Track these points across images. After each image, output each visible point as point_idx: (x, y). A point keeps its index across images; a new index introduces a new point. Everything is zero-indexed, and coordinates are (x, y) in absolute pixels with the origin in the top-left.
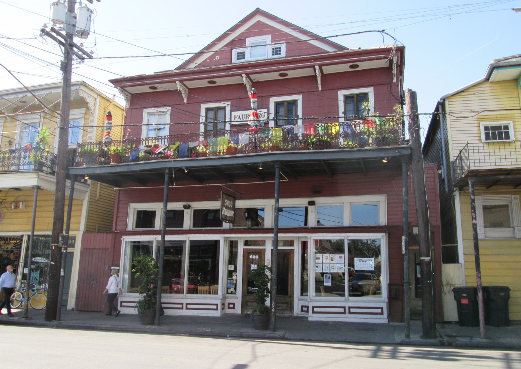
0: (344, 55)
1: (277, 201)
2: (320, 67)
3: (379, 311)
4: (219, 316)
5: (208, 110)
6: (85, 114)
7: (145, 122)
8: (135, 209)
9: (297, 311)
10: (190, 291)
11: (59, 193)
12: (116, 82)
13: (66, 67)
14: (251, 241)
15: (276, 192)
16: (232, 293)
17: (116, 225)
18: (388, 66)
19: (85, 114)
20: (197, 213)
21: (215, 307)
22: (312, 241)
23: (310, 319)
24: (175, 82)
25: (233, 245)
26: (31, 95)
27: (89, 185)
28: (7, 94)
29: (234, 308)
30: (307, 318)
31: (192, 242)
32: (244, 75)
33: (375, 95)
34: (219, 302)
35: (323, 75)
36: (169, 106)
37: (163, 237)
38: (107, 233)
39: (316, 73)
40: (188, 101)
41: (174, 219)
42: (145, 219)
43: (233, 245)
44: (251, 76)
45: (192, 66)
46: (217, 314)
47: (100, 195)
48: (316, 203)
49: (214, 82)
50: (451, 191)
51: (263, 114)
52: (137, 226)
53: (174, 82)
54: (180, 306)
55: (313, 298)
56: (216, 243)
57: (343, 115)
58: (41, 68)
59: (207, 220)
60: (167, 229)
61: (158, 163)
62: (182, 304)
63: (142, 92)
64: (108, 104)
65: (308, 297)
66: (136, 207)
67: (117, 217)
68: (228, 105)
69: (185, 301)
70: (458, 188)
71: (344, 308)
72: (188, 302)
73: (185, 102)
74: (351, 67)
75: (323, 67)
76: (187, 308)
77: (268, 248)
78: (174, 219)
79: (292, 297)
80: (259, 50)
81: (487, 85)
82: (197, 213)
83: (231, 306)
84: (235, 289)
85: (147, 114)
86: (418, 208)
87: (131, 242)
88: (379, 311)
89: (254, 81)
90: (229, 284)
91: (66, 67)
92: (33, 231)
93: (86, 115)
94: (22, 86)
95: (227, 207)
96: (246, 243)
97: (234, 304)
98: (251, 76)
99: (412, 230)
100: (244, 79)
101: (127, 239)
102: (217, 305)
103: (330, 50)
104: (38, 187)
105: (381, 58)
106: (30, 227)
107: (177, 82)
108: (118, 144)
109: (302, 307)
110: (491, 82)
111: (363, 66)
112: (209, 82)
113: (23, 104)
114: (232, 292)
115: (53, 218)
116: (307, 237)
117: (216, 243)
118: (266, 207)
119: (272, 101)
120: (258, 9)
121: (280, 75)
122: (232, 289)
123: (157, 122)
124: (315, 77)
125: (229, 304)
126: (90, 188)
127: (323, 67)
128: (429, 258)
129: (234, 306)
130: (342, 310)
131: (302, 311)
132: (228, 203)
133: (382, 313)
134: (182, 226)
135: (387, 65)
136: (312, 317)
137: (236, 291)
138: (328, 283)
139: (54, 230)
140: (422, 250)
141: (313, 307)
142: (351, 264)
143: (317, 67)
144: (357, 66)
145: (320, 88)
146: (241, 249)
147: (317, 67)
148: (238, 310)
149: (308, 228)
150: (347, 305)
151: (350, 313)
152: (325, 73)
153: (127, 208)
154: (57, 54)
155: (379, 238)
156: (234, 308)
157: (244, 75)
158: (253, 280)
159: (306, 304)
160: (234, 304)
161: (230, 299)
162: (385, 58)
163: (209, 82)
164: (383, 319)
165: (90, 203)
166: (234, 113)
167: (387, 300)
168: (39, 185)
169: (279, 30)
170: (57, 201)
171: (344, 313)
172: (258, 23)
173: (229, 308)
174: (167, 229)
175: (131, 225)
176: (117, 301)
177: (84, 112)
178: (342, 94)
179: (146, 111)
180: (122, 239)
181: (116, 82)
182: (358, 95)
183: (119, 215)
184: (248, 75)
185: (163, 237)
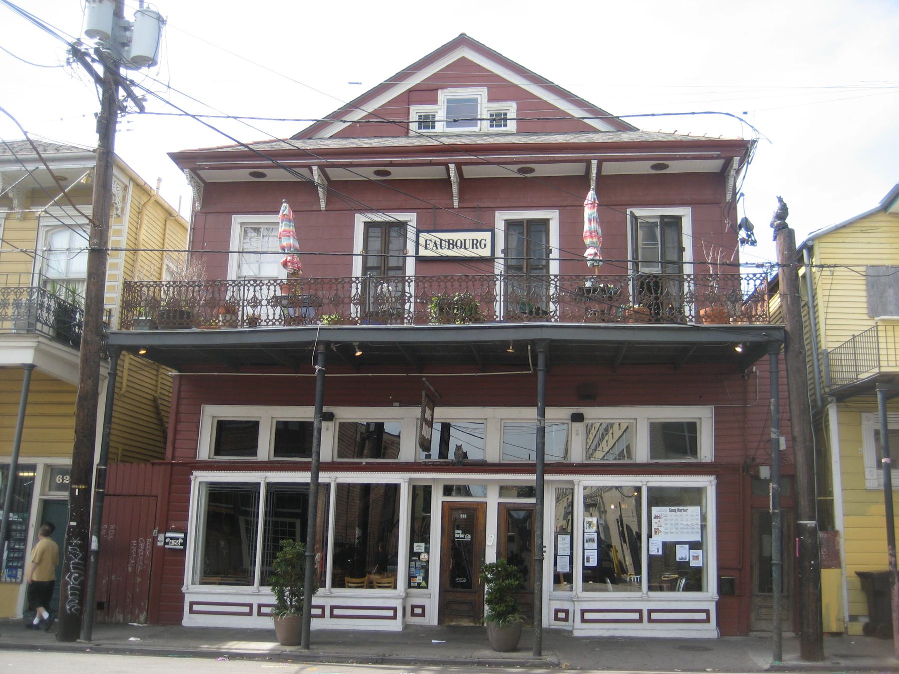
1: (542, 414)
2: (459, 166)
5: (368, 226)
6: (6, 219)
7: (234, 245)
8: (213, 417)
9: (547, 620)
11: (90, 382)
12: (183, 159)
16: (419, 586)
17: (174, 449)
18: (582, 173)
19: (6, 219)
20: (346, 431)
23: (577, 634)
25: (422, 495)
26: (45, 167)
29: (566, 619)
30: (571, 632)
31: (269, 485)
33: (694, 221)
34: (398, 604)
35: (464, 182)
37: (315, 477)
38: (153, 464)
39: (450, 177)
42: (236, 440)
43: (422, 495)
44: (328, 170)
46: (396, 626)
49: (263, 175)
50: (825, 403)
51: (483, 242)
52: (277, 452)
54: (247, 609)
55: (585, 597)
56: (395, 488)
57: (502, 256)
58: (64, 115)
59: (373, 444)
61: (578, 330)
63: (232, 181)
64: (145, 199)
65: (574, 592)
66: (213, 413)
67: (176, 432)
68: (410, 218)
70: (834, 399)
71: (640, 612)
72: (261, 602)
73: (456, 205)
74: (654, 167)
75: (464, 168)
77: (493, 503)
78: (295, 441)
80: (488, 121)
81: (882, 217)
82: (346, 431)
83: (418, 611)
84: (426, 578)
85: (239, 226)
86: (796, 434)
87: (207, 483)
88: (703, 616)
89: (333, 179)
90: (413, 570)
93: (7, 221)
94: (234, 143)
96: (448, 490)
97: (423, 608)
98: (328, 170)
99: (758, 472)
101: (200, 478)
102: (707, 612)
104: (31, 367)
105: (712, 158)
109: (557, 611)
110: (890, 213)
111: (676, 167)
112: (252, 174)
113: (41, 184)
114: (419, 584)
115: (73, 431)
116: (572, 482)
117: (395, 488)
118: (400, 421)
119: (501, 218)
120: (462, 34)
122: (419, 579)
123: (262, 255)
124: (448, 182)
127: (464, 168)
128: (814, 522)
130: (636, 616)
131: (556, 618)
133: (707, 620)
134: (255, 454)
135: (582, 173)
136: (582, 630)
137: (427, 583)
139: (76, 456)
141: (583, 612)
142: (7, 517)
143: (594, 163)
144: (666, 167)
146: (438, 500)
147: (594, 163)
148: (432, 618)
149: (571, 465)
150: (645, 607)
151: (650, 620)
152: (466, 176)
153: (198, 414)
156: (423, 615)
157: (315, 168)
158: (461, 561)
159: (566, 605)
161: (418, 598)
162: (718, 157)
163: (252, 174)
164: (710, 630)
166: (423, 236)
167: (716, 597)
168: (35, 364)
169: (517, 87)
170: (82, 399)
171: (640, 620)
172: (460, 64)
173: (413, 614)
175: (205, 450)
176: (183, 602)
178: (360, 220)
179: (237, 220)
180: (192, 477)
181: (183, 159)
182: (530, 222)
183: (180, 427)
184: (322, 168)
185: (315, 477)
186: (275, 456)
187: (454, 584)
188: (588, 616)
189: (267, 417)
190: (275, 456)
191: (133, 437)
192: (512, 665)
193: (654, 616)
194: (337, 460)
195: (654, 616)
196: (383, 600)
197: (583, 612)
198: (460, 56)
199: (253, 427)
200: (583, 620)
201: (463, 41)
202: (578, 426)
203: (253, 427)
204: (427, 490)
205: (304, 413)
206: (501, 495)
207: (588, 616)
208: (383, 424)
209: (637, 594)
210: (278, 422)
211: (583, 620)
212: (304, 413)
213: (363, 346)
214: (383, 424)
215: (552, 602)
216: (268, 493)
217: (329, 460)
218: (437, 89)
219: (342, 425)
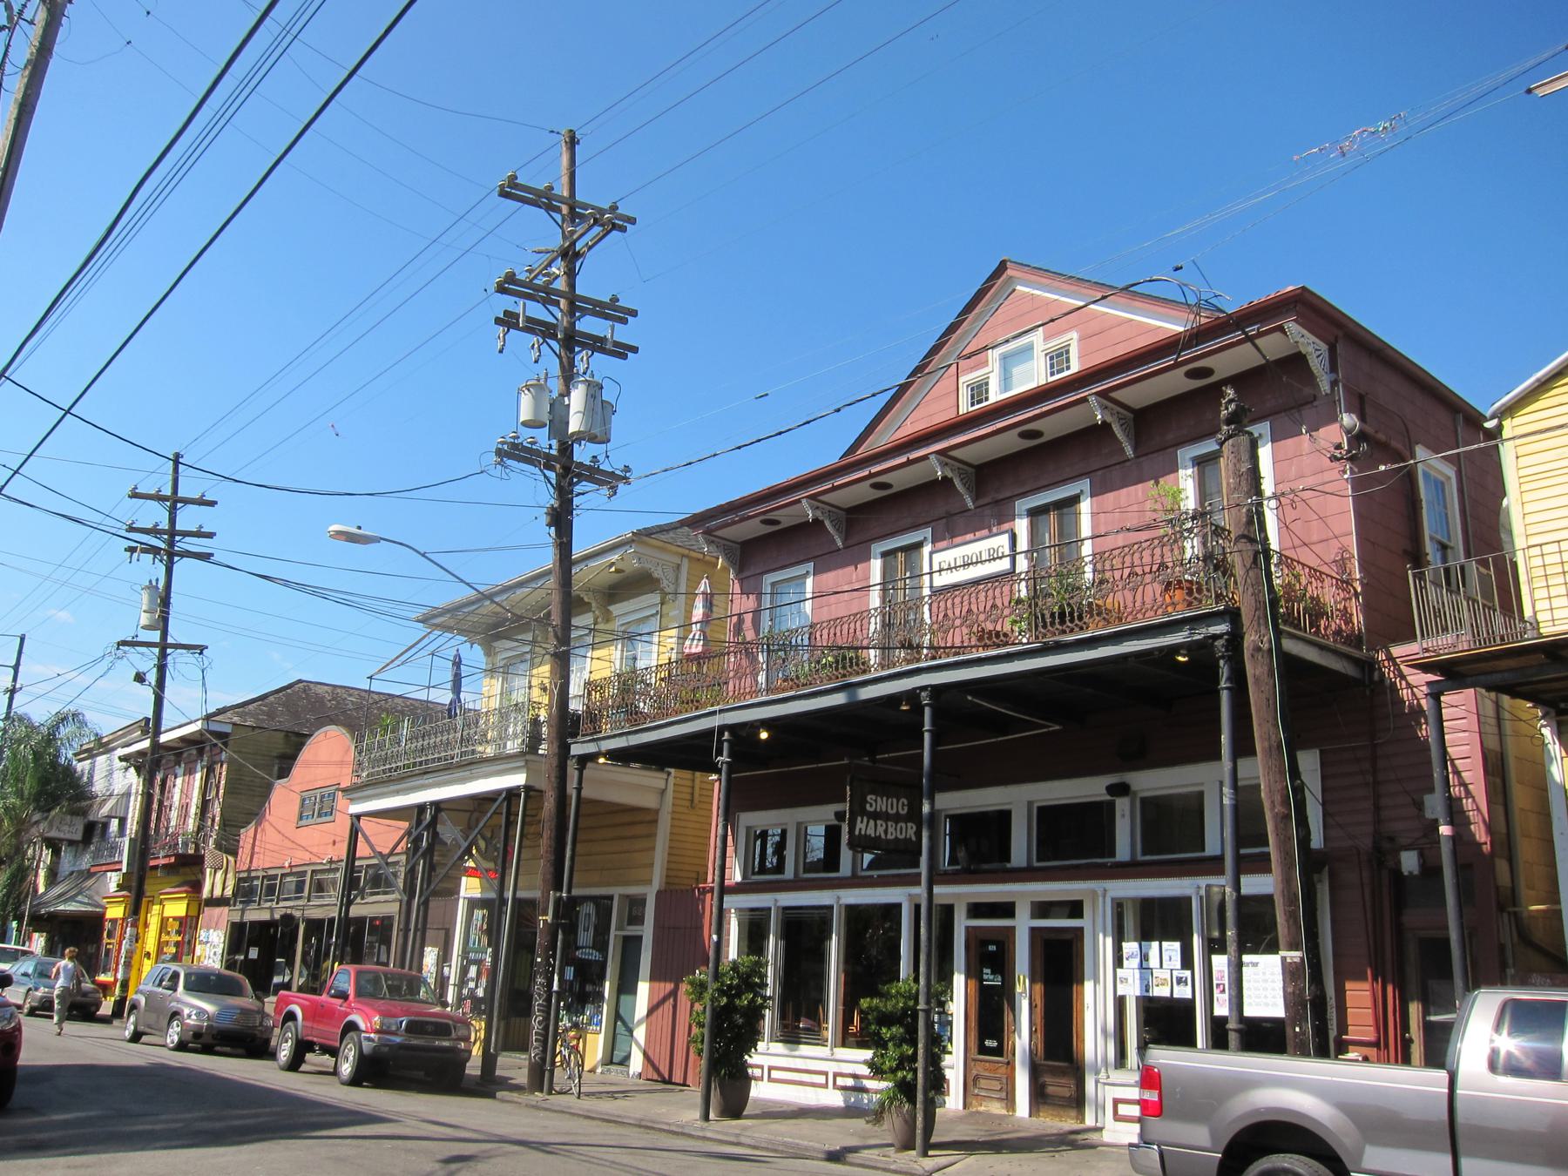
13: (561, 519)
15: (1225, 739)
24: (798, 501)
28: (506, 589)
36: (925, 524)
40: (1135, 449)
43: (410, 968)
48: (1133, 788)
60: (1243, 851)
62: (826, 1074)
73: (970, 505)
91: (561, 519)
108: (950, 613)
112: (1024, 435)
128: (1298, 954)
138: (989, 1043)
140: (1109, 941)
141: (1116, 1102)
145: (1129, 451)
154: (537, 489)
174: (1243, 851)
177: (658, 600)
187: (983, 1050)
189: (1019, 800)
192: (749, 1146)
193: (775, 1074)
194: (1140, 858)
195: (775, 1074)
197: (1116, 1102)
199: (1003, 818)
202: (1122, 805)
203: (1003, 818)
204: (948, 911)
205: (1090, 789)
206: (1034, 916)
210: (1040, 809)
212: (1090, 789)
213: (766, 723)
217: (1024, 864)
219: (1144, 801)
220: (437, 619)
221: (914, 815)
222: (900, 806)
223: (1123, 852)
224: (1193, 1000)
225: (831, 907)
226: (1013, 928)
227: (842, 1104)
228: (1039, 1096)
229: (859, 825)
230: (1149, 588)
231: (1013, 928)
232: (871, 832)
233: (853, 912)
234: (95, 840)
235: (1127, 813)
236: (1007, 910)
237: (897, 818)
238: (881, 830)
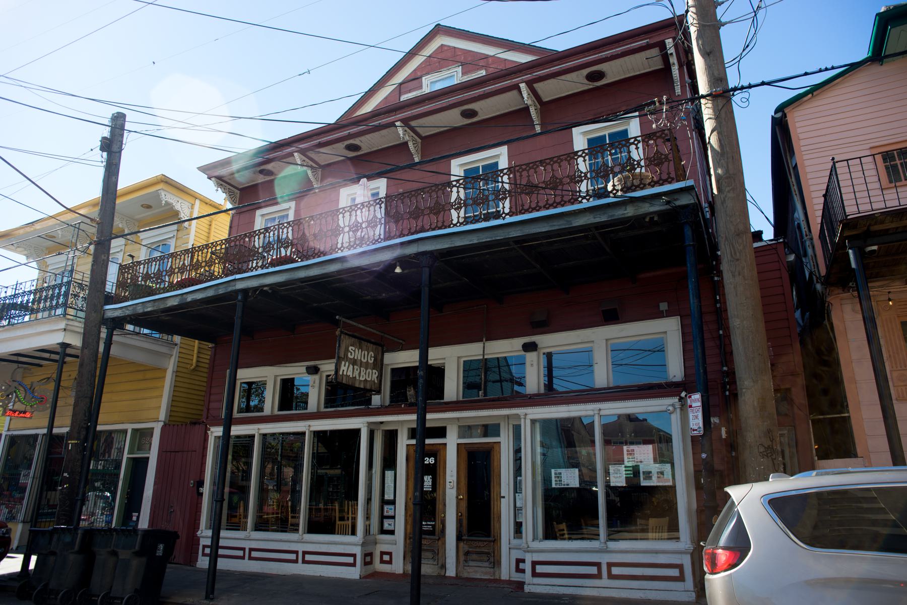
0: (549, 62)
2: (530, 84)
3: (675, 572)
4: (357, 577)
9: (506, 571)
10: (313, 528)
14: (273, 434)
21: (350, 560)
22: (528, 423)
24: (392, 125)
27: (176, 345)
29: (390, 562)
32: (398, 124)
34: (358, 551)
35: (545, 106)
41: (290, 397)
45: (368, 108)
46: (354, 573)
47: (198, 361)
53: (291, 155)
54: (293, 557)
59: (341, 395)
62: (296, 552)
69: (301, 548)
75: (536, 86)
76: (304, 562)
79: (497, 540)
83: (386, 558)
92: (51, 426)
93: (305, 202)
95: (354, 362)
97: (390, 554)
100: (400, 131)
102: (354, 556)
103: (523, 58)
106: (46, 422)
107: (296, 154)
116: (517, 416)
117: (355, 434)
121: (592, 77)
124: (525, 111)
125: (382, 553)
126: (175, 351)
127: (536, 86)
129: (391, 558)
132: (355, 353)
135: (658, 65)
143: (523, 86)
146: (403, 443)
147: (523, 86)
155: (591, 413)
156: (390, 562)
157: (398, 124)
160: (390, 554)
161: (384, 543)
165: (177, 373)
171: (296, 561)
173: (382, 561)
184: (406, 122)
186: (326, 407)
188: (540, 569)
189: (451, 358)
190: (326, 407)
191: (192, 406)
193: (254, 554)
194: (323, 409)
196: (342, 546)
197: (534, 564)
198: (439, 45)
200: (535, 574)
201: (439, 30)
202: (531, 357)
207: (540, 569)
208: (293, 379)
209: (594, 544)
211: (535, 574)
214: (293, 379)
215: (513, 551)
216: (464, 437)
217: (455, 399)
218: (421, 77)
220: (203, 169)
221: (379, 365)
222: (368, 357)
223: (267, 410)
224: (673, 488)
225: (304, 434)
226: (445, 444)
227: (401, 572)
228: (464, 557)
229: (343, 368)
230: (347, 224)
231: (445, 444)
232: (350, 373)
233: (320, 436)
234: (339, 254)
235: (535, 363)
236: (441, 432)
237: (367, 366)
238: (356, 373)
